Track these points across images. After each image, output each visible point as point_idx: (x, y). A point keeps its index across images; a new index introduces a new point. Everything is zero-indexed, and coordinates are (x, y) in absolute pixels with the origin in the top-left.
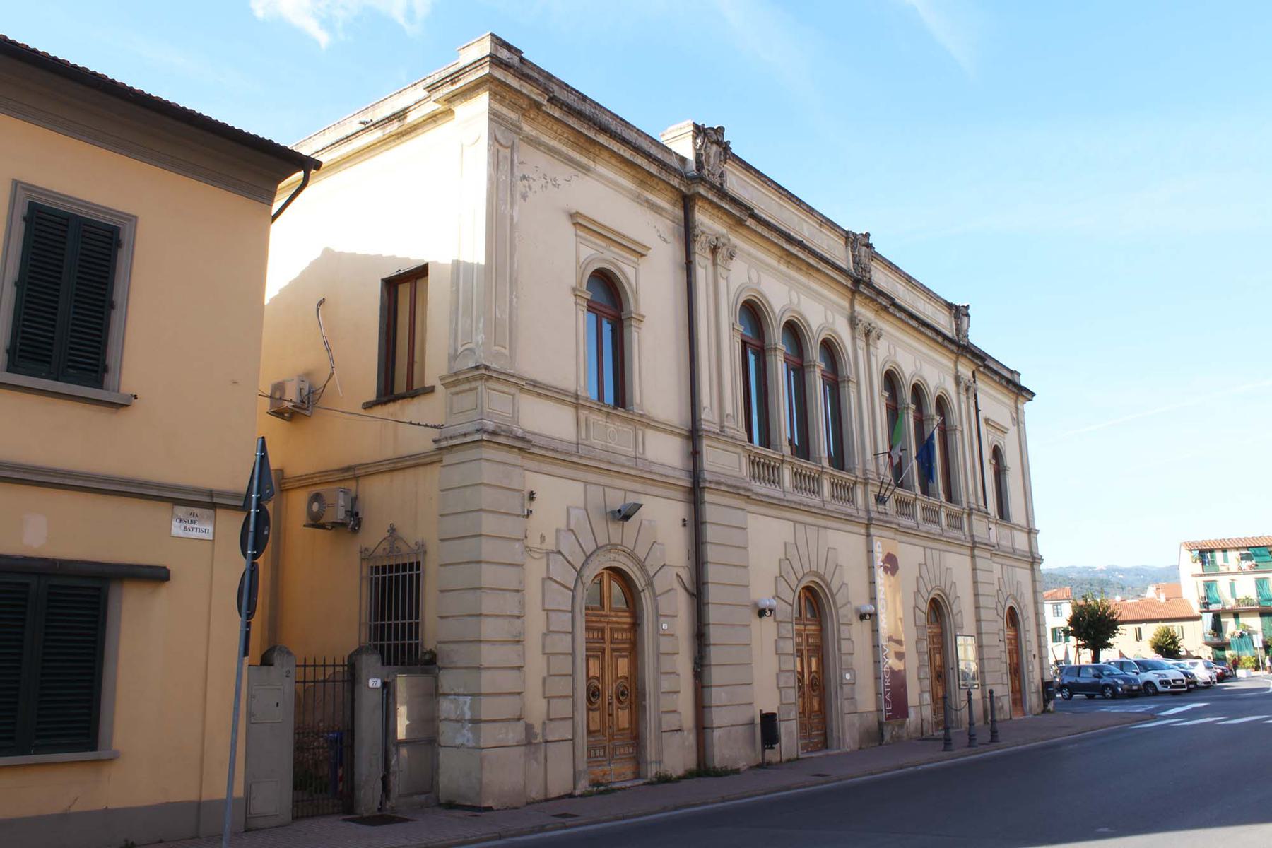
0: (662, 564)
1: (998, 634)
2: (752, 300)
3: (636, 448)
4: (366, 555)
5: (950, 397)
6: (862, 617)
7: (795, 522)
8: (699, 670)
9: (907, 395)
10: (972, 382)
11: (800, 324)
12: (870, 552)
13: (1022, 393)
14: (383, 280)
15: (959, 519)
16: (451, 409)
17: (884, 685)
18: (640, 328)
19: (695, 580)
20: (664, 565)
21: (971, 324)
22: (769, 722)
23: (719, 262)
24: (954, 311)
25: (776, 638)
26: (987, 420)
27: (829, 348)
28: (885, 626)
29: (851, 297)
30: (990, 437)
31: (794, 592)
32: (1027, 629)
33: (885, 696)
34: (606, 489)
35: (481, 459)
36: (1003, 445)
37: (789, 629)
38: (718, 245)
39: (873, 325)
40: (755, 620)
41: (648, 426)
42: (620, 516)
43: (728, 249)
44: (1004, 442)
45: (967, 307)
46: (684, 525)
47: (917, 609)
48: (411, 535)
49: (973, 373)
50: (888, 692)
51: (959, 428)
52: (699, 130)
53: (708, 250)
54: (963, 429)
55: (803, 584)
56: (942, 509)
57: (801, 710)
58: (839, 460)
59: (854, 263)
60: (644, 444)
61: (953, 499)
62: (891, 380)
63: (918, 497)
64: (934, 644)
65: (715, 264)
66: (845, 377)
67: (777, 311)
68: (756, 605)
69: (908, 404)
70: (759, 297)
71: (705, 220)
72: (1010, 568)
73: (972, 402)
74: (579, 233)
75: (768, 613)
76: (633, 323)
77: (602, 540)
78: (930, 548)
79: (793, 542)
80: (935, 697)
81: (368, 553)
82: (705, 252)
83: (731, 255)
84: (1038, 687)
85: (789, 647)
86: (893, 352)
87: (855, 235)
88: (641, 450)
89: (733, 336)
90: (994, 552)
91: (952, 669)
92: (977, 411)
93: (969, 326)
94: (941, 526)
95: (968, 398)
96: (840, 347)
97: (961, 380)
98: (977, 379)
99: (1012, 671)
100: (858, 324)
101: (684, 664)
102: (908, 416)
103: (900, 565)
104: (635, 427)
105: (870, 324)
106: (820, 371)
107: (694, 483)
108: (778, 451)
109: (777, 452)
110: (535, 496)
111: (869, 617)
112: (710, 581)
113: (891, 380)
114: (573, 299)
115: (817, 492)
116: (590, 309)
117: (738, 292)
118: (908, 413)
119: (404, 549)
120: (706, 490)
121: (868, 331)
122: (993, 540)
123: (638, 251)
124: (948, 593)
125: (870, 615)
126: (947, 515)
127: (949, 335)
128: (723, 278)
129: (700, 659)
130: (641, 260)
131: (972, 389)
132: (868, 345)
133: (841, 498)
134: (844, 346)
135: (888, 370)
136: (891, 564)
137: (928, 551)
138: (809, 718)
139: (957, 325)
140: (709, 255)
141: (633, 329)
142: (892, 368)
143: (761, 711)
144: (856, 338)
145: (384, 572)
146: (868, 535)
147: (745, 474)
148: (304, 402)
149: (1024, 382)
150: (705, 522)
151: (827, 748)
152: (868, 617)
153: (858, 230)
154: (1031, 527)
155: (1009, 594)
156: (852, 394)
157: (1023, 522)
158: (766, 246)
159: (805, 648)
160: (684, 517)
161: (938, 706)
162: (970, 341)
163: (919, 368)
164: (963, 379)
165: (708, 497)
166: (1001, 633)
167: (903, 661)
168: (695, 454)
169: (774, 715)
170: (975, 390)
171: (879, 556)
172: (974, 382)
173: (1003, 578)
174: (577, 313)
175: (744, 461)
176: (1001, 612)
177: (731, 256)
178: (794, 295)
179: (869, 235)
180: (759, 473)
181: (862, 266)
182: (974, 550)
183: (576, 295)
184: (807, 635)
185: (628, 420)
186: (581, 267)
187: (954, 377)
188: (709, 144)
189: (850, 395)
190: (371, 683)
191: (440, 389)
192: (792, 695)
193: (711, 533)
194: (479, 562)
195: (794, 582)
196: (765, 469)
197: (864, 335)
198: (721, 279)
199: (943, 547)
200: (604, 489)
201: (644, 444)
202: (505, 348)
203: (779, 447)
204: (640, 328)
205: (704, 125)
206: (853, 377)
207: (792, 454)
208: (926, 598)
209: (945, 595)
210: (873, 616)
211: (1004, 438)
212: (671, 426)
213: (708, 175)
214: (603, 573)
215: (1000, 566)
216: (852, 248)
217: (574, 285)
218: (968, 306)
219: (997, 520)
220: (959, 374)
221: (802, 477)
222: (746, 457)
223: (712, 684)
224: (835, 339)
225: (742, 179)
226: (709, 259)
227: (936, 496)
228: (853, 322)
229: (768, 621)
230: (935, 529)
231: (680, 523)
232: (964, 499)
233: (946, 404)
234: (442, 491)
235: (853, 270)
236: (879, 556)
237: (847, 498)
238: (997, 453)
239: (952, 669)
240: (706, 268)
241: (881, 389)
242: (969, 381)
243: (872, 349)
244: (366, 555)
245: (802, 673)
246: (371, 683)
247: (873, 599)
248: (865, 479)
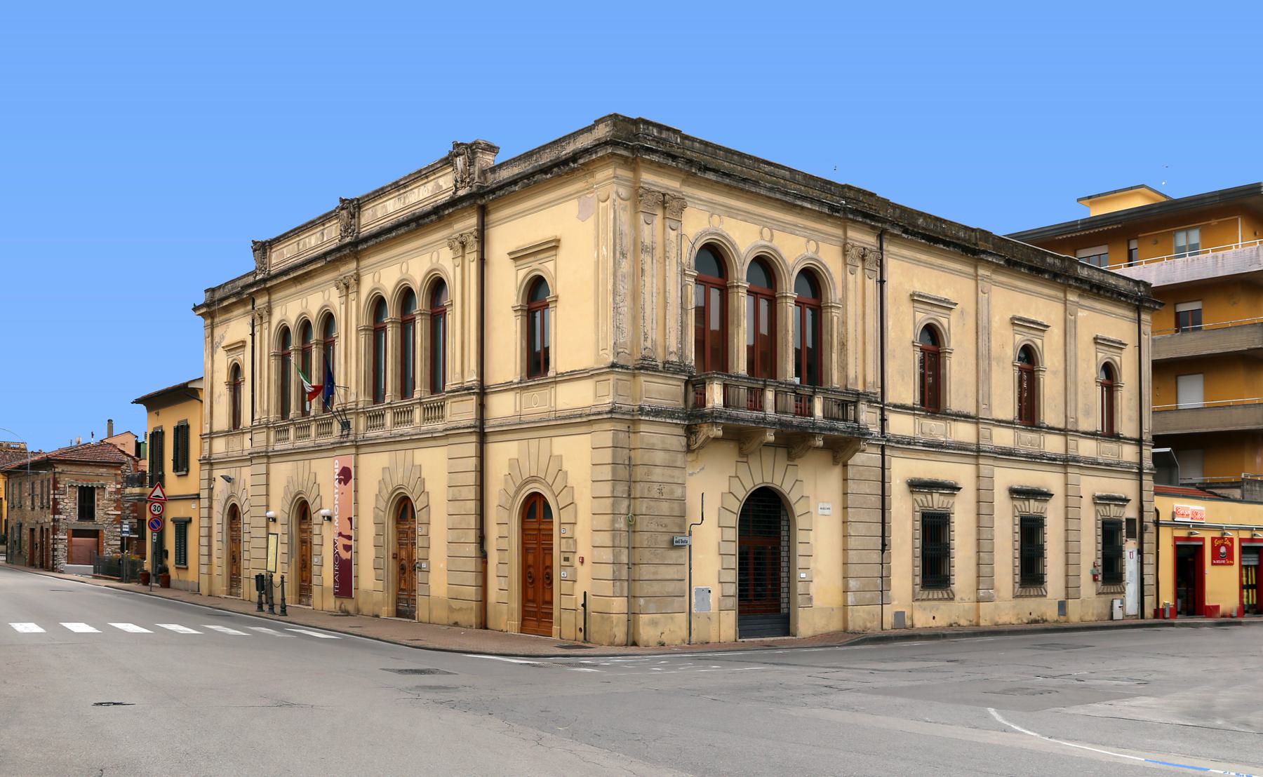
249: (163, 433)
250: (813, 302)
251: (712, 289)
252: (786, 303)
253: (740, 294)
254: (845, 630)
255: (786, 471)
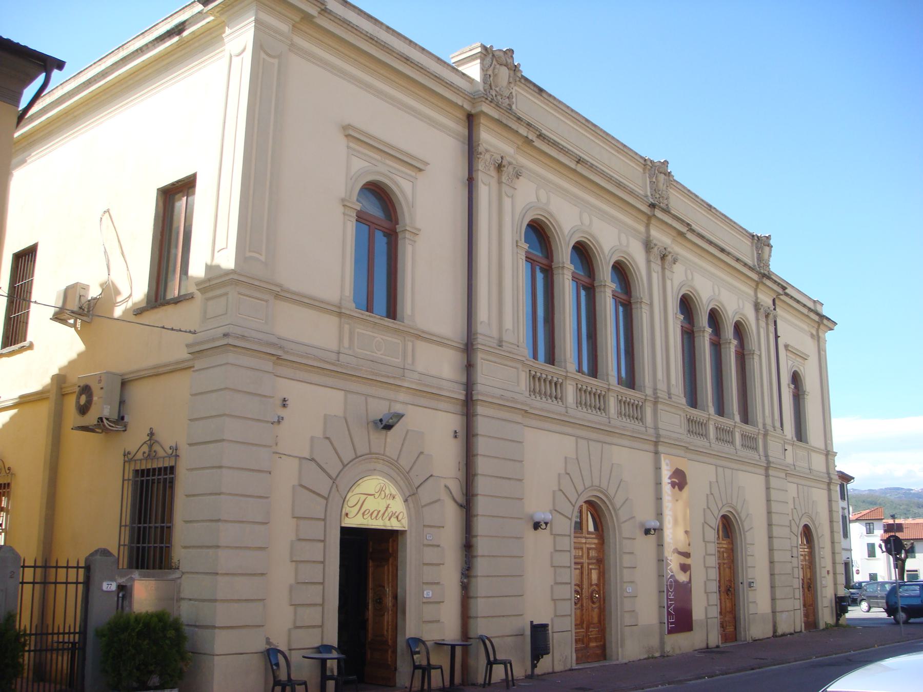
0: (430, 475)
1: (791, 551)
2: (717, 310)
3: (404, 360)
4: (128, 458)
5: (749, 322)
6: (647, 532)
7: (578, 437)
8: (465, 580)
9: (703, 320)
10: (772, 309)
11: (628, 264)
12: (658, 468)
13: (822, 322)
14: (158, 189)
15: (755, 440)
16: (205, 312)
17: (667, 598)
18: (415, 242)
19: (465, 492)
20: (431, 476)
21: (772, 254)
22: (539, 633)
23: (666, 266)
24: (756, 241)
25: (552, 551)
26: (786, 347)
27: (621, 271)
28: (671, 541)
29: (646, 222)
30: (790, 363)
31: (574, 506)
32: (821, 546)
33: (668, 607)
34: (799, 486)
35: (227, 364)
36: (803, 371)
37: (566, 543)
38: (503, 164)
39: (669, 249)
40: (531, 534)
41: (418, 337)
42: (382, 426)
43: (673, 256)
44: (804, 369)
45: (768, 238)
46: (456, 437)
47: (706, 525)
48: (167, 439)
49: (774, 300)
50: (671, 605)
51: (757, 352)
52: (487, 53)
53: (492, 168)
54: (761, 353)
55: (585, 497)
56: (736, 429)
57: (578, 622)
58: (630, 380)
59: (651, 189)
60: (413, 356)
61: (726, 411)
62: (687, 305)
63: (711, 417)
64: (724, 559)
65: (500, 182)
66: (727, 339)
67: (566, 232)
68: (531, 518)
69: (704, 327)
70: (589, 238)
71: (487, 137)
72: (805, 488)
73: (772, 328)
74: (352, 145)
75: (544, 526)
76: (407, 236)
77: (362, 449)
78: (802, 485)
79: (574, 457)
80: (723, 611)
81: (130, 457)
82: (489, 170)
83: (675, 261)
84: (831, 601)
85: (566, 559)
86: (690, 277)
87: (651, 162)
88: (409, 361)
89: (517, 253)
90: (788, 472)
91: (742, 583)
92: (777, 337)
93: (770, 256)
94: (734, 446)
95: (767, 324)
96: (634, 270)
97: (652, 245)
98: (777, 306)
99: (805, 586)
100: (760, 309)
101: (450, 577)
102: (704, 339)
103: (688, 481)
104: (405, 338)
105: (665, 249)
106: (610, 292)
107: (467, 395)
108: (604, 381)
109: (560, 369)
110: (287, 402)
111: (653, 532)
112: (479, 492)
113: (687, 305)
114: (341, 209)
115: (602, 409)
116: (360, 220)
117: (524, 211)
118: (704, 336)
119: (161, 453)
120: (479, 402)
121: (664, 255)
122: (789, 459)
123: (416, 167)
124: (740, 510)
125: (655, 530)
126: (742, 435)
127: (750, 262)
128: (655, 272)
129: (467, 570)
130: (420, 176)
131: (771, 316)
132: (663, 268)
133: (595, 407)
134: (750, 325)
135: (737, 321)
136: (680, 480)
137: (720, 470)
138: (588, 628)
139: (759, 254)
140: (659, 262)
141: (407, 241)
142: (740, 319)
143: (532, 622)
144: (651, 261)
145: (148, 475)
146: (657, 453)
147: (524, 389)
148: (83, 310)
149: (825, 312)
150: (477, 435)
151: (736, 641)
152: (652, 532)
153: (657, 158)
154: (828, 449)
155: (803, 512)
156: (644, 315)
157: (820, 444)
158: (499, 131)
159: (585, 560)
160: (456, 429)
161: (727, 619)
162: (771, 270)
163: (741, 307)
164: (762, 305)
165: (480, 409)
166: (795, 550)
167: (688, 573)
168: (469, 367)
169: (544, 627)
170: (775, 317)
171: (666, 473)
172: (775, 309)
173: (798, 497)
174: (344, 223)
175: (524, 377)
176: (795, 529)
177: (518, 175)
178: (586, 218)
179: (668, 163)
180: (545, 389)
181: (660, 192)
182: (768, 470)
183: (344, 206)
184: (588, 548)
185: (396, 331)
186: (351, 179)
187: (753, 303)
188: (498, 66)
189: (643, 316)
190: (105, 586)
191: (198, 295)
192: (568, 608)
193: (482, 445)
194: (220, 467)
195: (716, 513)
196: (696, 427)
197: (764, 317)
198: (482, 184)
199: (733, 465)
200: (366, 399)
201: (413, 356)
202: (261, 255)
203: (563, 364)
204: (415, 242)
205: (492, 46)
206: (646, 300)
207: (618, 384)
208: (716, 513)
209: (602, 492)
210: (659, 531)
211: (804, 364)
212: (261, 281)
213: (496, 96)
214: (582, 505)
215: (796, 485)
216: (650, 175)
217: (343, 195)
218: (770, 236)
219: (794, 441)
220: (759, 301)
221: (623, 404)
222: (526, 372)
223: (479, 595)
224: (744, 321)
225: (723, 227)
226: (659, 265)
227: (731, 417)
228: (648, 246)
229: (541, 533)
230: (727, 448)
231: (452, 434)
232: (760, 420)
233: (745, 329)
234: (192, 395)
235: (757, 266)
236: (666, 473)
237: (694, 431)
238: (796, 379)
239: (742, 583)
240: (658, 272)
241: (675, 312)
242: (769, 308)
243: (667, 272)
244: (128, 458)
245: (580, 585)
246: (105, 586)
247: (659, 515)
248: (655, 398)
249: (844, 537)
250: (386, 224)
251: (377, 231)
252: (563, 274)
253: (565, 276)
254: (707, 648)
255: (367, 410)
